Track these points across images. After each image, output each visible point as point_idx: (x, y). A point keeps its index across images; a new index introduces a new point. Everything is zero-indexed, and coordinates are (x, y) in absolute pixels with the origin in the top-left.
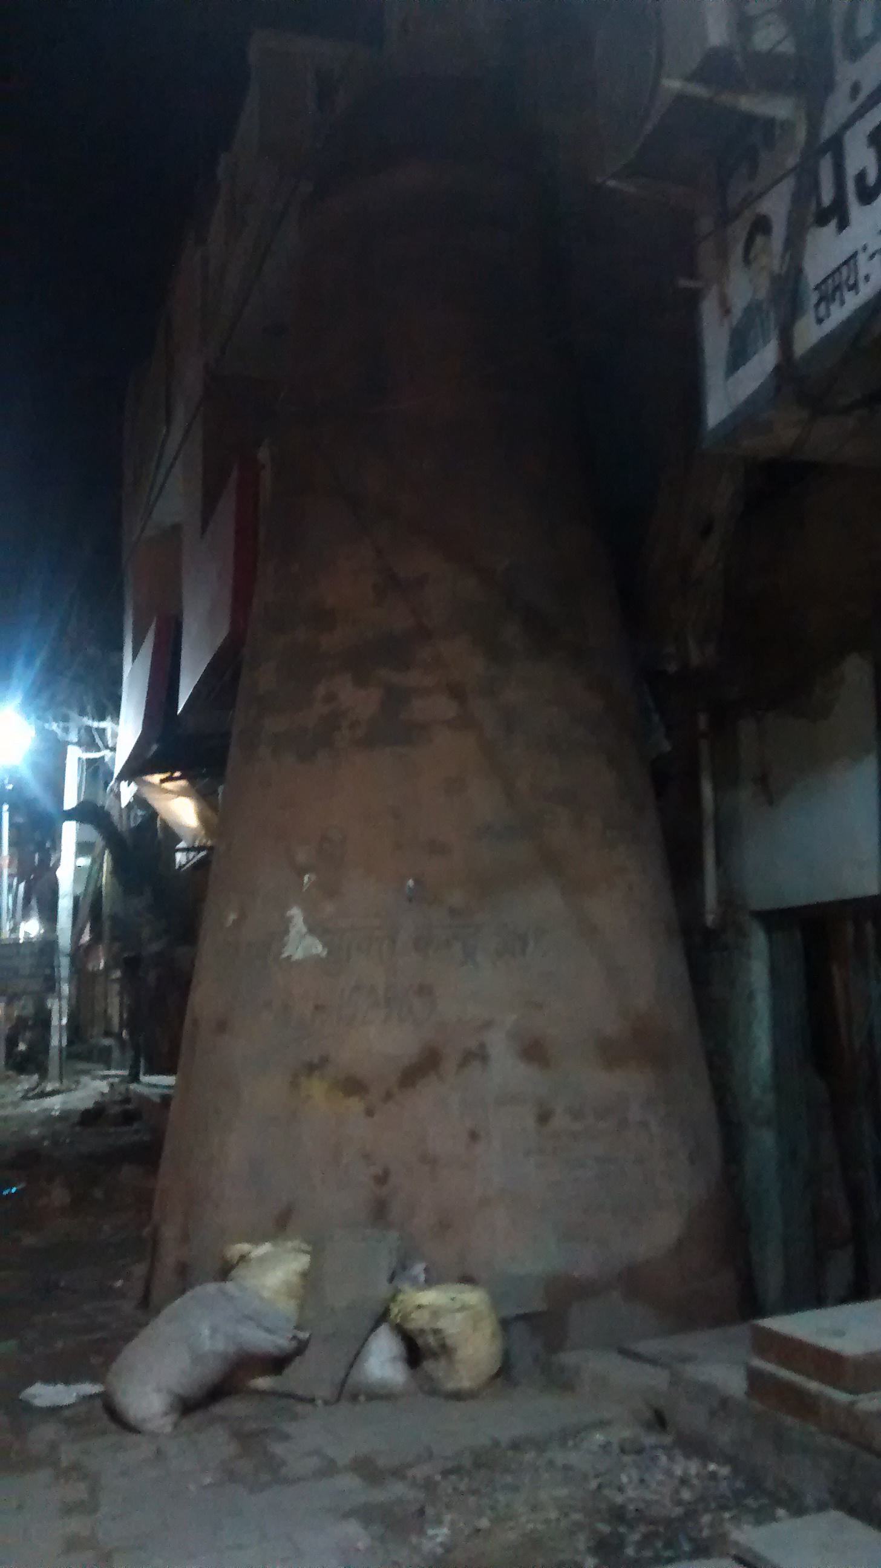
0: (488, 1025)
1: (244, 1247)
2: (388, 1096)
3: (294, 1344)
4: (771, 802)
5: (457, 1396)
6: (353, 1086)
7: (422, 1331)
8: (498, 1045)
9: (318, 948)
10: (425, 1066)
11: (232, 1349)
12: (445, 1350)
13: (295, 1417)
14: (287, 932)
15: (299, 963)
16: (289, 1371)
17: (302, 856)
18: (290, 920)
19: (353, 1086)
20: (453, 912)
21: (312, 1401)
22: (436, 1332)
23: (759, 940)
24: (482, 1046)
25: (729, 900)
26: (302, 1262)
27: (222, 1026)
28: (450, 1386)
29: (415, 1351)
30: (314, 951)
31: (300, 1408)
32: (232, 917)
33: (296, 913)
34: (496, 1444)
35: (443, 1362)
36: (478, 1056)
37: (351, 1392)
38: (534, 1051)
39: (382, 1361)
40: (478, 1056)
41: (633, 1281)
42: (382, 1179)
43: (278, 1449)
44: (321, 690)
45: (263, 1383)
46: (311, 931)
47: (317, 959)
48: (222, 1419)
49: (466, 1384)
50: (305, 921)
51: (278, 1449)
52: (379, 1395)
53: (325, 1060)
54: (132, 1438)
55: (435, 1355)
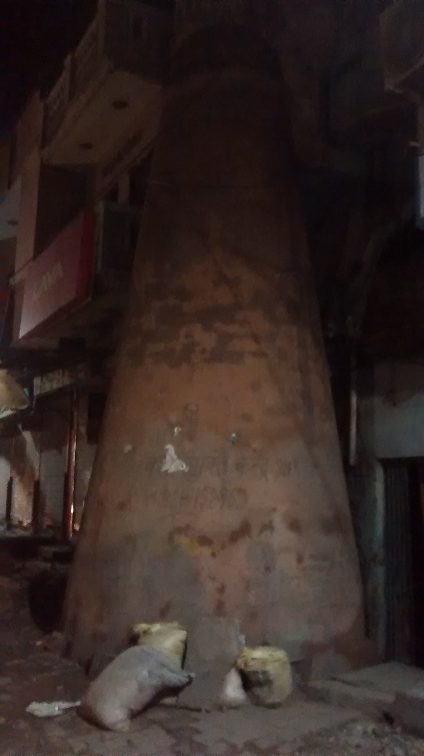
0: (274, 510)
1: (143, 626)
2: (223, 547)
3: (187, 680)
4: (395, 404)
5: (273, 706)
6: (204, 541)
7: (256, 673)
8: (278, 521)
9: (183, 467)
10: (244, 530)
11: (156, 682)
12: (267, 682)
13: (196, 720)
14: (165, 457)
15: (173, 475)
16: (181, 695)
17: (173, 418)
18: (167, 450)
19: (204, 541)
20: (255, 450)
21: (199, 710)
22: (265, 673)
23: (379, 473)
24: (271, 522)
25: (362, 450)
26: (180, 635)
27: (122, 506)
28: (270, 701)
29: (248, 681)
30: (181, 468)
31: (195, 714)
32: (128, 448)
33: (170, 448)
34: (311, 733)
35: (266, 688)
36: (268, 527)
37: (222, 707)
38: (295, 526)
39: (233, 690)
40: (268, 527)
41: (338, 644)
42: (222, 590)
43: (197, 738)
44: (183, 331)
45: (169, 700)
46: (179, 457)
47: (183, 472)
48: (154, 722)
49: (277, 700)
50: (176, 452)
51: (197, 738)
52: (234, 707)
53: (188, 527)
54: (107, 735)
55: (260, 684)
